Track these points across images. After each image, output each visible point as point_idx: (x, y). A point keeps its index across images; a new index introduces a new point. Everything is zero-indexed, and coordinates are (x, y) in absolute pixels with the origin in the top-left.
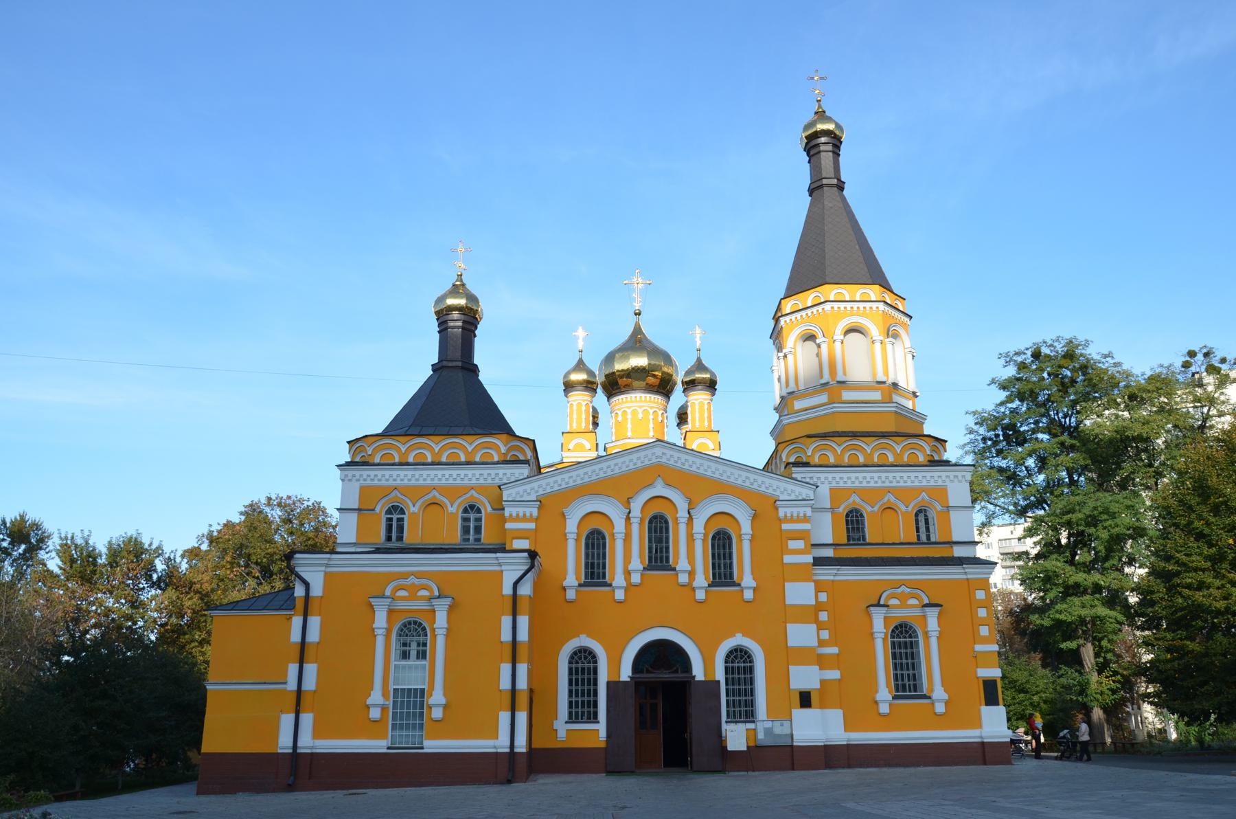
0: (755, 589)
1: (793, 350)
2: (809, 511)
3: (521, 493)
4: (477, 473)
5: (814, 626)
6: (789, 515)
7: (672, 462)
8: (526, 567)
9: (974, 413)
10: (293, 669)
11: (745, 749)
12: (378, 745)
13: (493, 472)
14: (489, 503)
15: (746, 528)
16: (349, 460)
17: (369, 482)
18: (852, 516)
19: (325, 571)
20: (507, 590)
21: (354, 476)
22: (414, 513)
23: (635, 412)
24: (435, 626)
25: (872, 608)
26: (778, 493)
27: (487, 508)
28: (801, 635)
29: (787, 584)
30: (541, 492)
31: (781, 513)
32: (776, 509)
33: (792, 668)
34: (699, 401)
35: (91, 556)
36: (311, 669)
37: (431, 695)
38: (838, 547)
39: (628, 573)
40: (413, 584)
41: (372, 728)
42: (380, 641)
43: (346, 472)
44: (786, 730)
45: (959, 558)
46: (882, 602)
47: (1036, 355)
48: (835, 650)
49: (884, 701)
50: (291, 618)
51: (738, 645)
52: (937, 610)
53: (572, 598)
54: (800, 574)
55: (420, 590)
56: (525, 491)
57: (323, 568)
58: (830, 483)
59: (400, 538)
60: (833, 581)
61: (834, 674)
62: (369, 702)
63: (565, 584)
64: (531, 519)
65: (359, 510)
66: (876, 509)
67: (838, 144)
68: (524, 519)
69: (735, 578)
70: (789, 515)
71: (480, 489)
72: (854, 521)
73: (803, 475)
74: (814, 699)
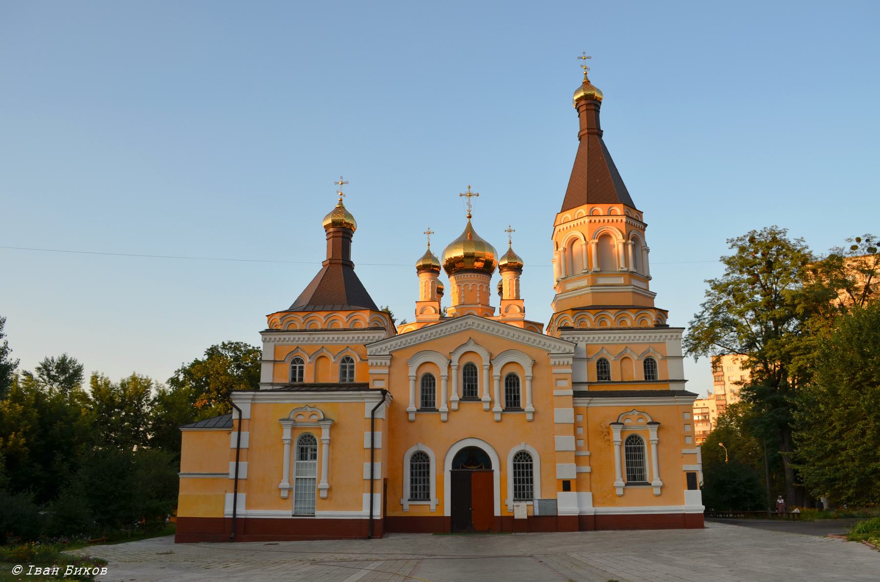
2: (571, 361)
20: (368, 415)
21: (270, 339)
47: (752, 240)
59: (301, 380)
65: (275, 361)
72: (603, 367)
74: (573, 485)
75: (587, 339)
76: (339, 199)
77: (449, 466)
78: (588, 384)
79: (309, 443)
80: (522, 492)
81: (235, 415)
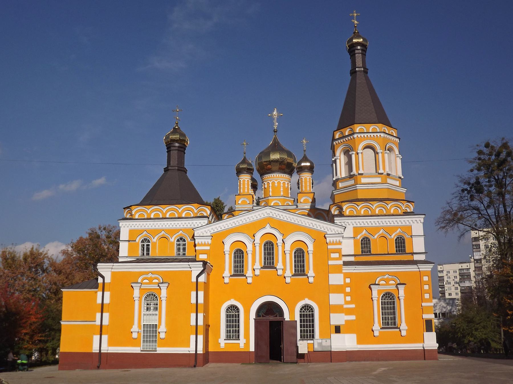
5: (343, 295)
9: (458, 176)
10: (98, 315)
15: (311, 247)
17: (133, 227)
20: (194, 280)
24: (161, 296)
26: (326, 230)
27: (188, 240)
28: (336, 299)
29: (330, 275)
30: (212, 232)
35: (13, 259)
36: (106, 315)
41: (134, 342)
42: (137, 303)
44: (328, 344)
45: (416, 260)
47: (487, 146)
49: (376, 330)
51: (306, 304)
53: (108, 314)
54: (337, 269)
57: (110, 270)
58: (353, 224)
62: (132, 330)
65: (129, 241)
67: (365, 49)
68: (205, 245)
69: (306, 272)
71: (185, 230)
72: (366, 243)
73: (340, 221)
74: (334, 329)
77: (253, 315)
80: (309, 334)
81: (100, 280)
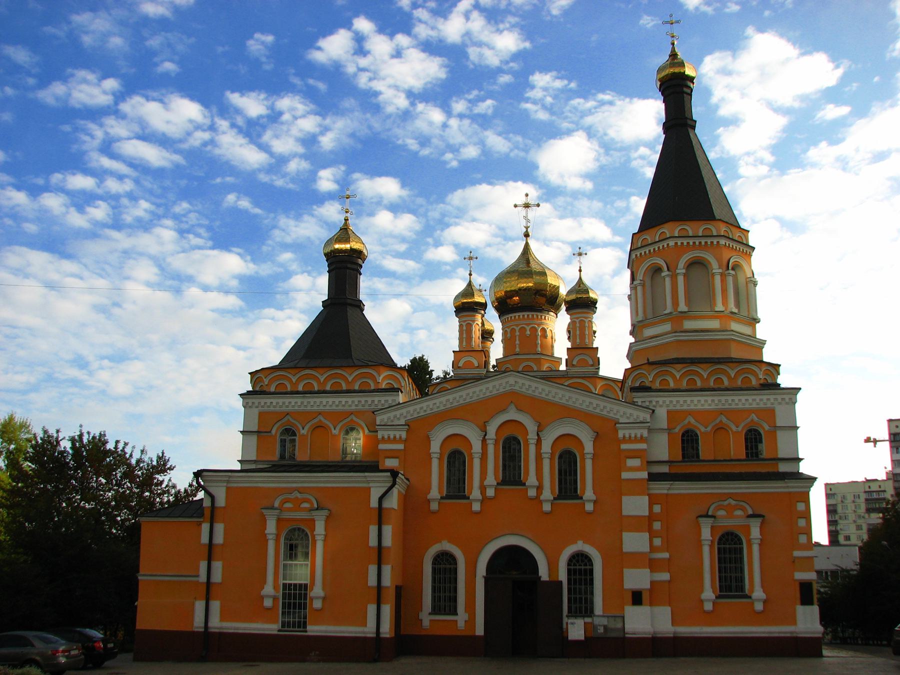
0: (595, 502)
1: (642, 282)
2: (645, 433)
3: (392, 419)
4: (356, 400)
6: (627, 436)
7: (524, 390)
8: (389, 485)
10: (203, 565)
11: (582, 638)
12: (271, 628)
13: (369, 400)
14: (367, 426)
15: (589, 447)
16: (250, 389)
18: (688, 436)
19: (226, 486)
20: (374, 503)
21: (253, 403)
22: (303, 435)
23: (523, 330)
24: (315, 533)
25: (700, 519)
30: (409, 417)
31: (621, 434)
32: (616, 431)
33: (625, 571)
34: (580, 319)
36: (217, 566)
37: (313, 590)
38: (673, 464)
39: (483, 489)
40: (297, 497)
43: (248, 400)
44: (619, 625)
46: (710, 513)
48: (666, 555)
49: (708, 600)
50: (201, 524)
52: (759, 520)
54: (635, 488)
55: (302, 502)
56: (395, 416)
57: (225, 484)
60: (667, 495)
61: (665, 576)
62: (263, 592)
63: (429, 497)
64: (400, 441)
65: (258, 432)
66: (709, 429)
68: (395, 440)
70: (627, 436)
73: (643, 400)
74: (645, 597)
75: (710, 403)
76: (851, 164)
78: (669, 464)
79: (733, 543)
